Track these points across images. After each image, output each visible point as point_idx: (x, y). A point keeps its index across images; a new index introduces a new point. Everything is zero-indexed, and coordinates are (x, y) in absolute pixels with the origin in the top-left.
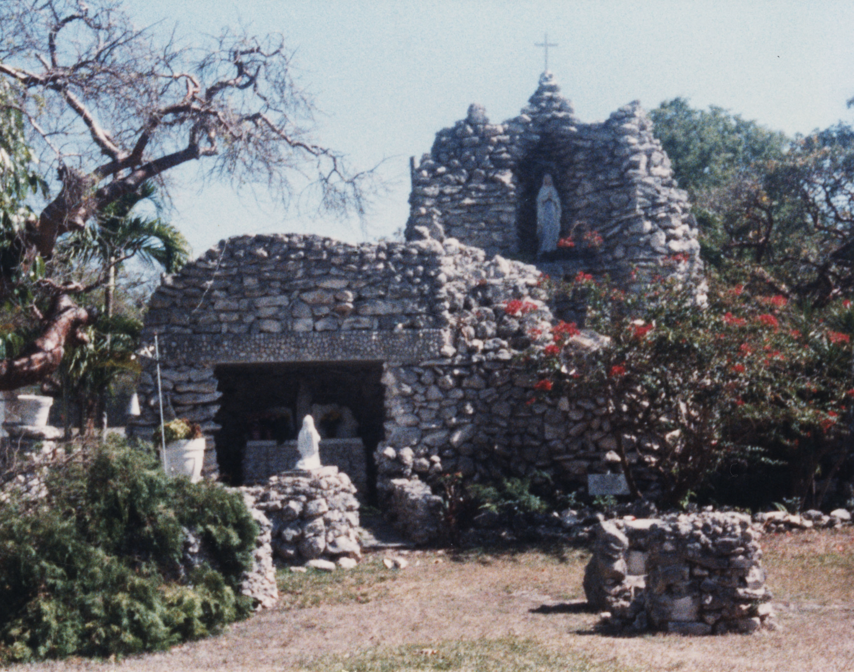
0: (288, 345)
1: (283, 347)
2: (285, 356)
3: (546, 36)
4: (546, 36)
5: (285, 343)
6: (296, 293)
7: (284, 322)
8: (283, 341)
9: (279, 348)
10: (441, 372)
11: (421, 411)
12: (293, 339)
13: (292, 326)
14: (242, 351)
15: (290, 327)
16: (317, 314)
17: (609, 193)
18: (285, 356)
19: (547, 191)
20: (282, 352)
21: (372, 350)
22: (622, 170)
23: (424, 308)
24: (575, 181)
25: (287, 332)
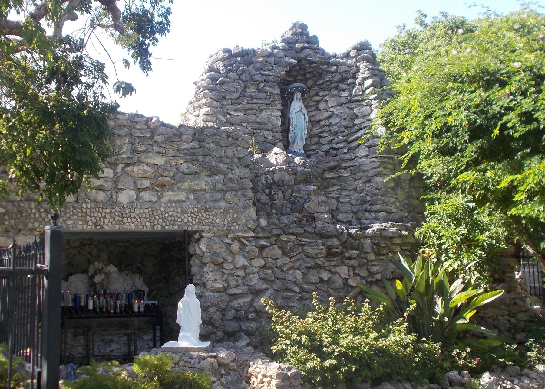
0: (113, 215)
1: (108, 216)
2: (110, 224)
3: (147, 75)
4: (147, 75)
5: (111, 212)
6: (120, 166)
7: (109, 193)
8: (108, 211)
9: (105, 217)
10: (246, 242)
11: (230, 278)
12: (118, 209)
13: (117, 197)
14: (70, 219)
15: (114, 198)
16: (139, 187)
17: (353, 105)
18: (110, 224)
19: (297, 105)
20: (106, 221)
21: (189, 221)
22: (364, 89)
23: (25, 177)
24: (317, 98)
25: (113, 203)
